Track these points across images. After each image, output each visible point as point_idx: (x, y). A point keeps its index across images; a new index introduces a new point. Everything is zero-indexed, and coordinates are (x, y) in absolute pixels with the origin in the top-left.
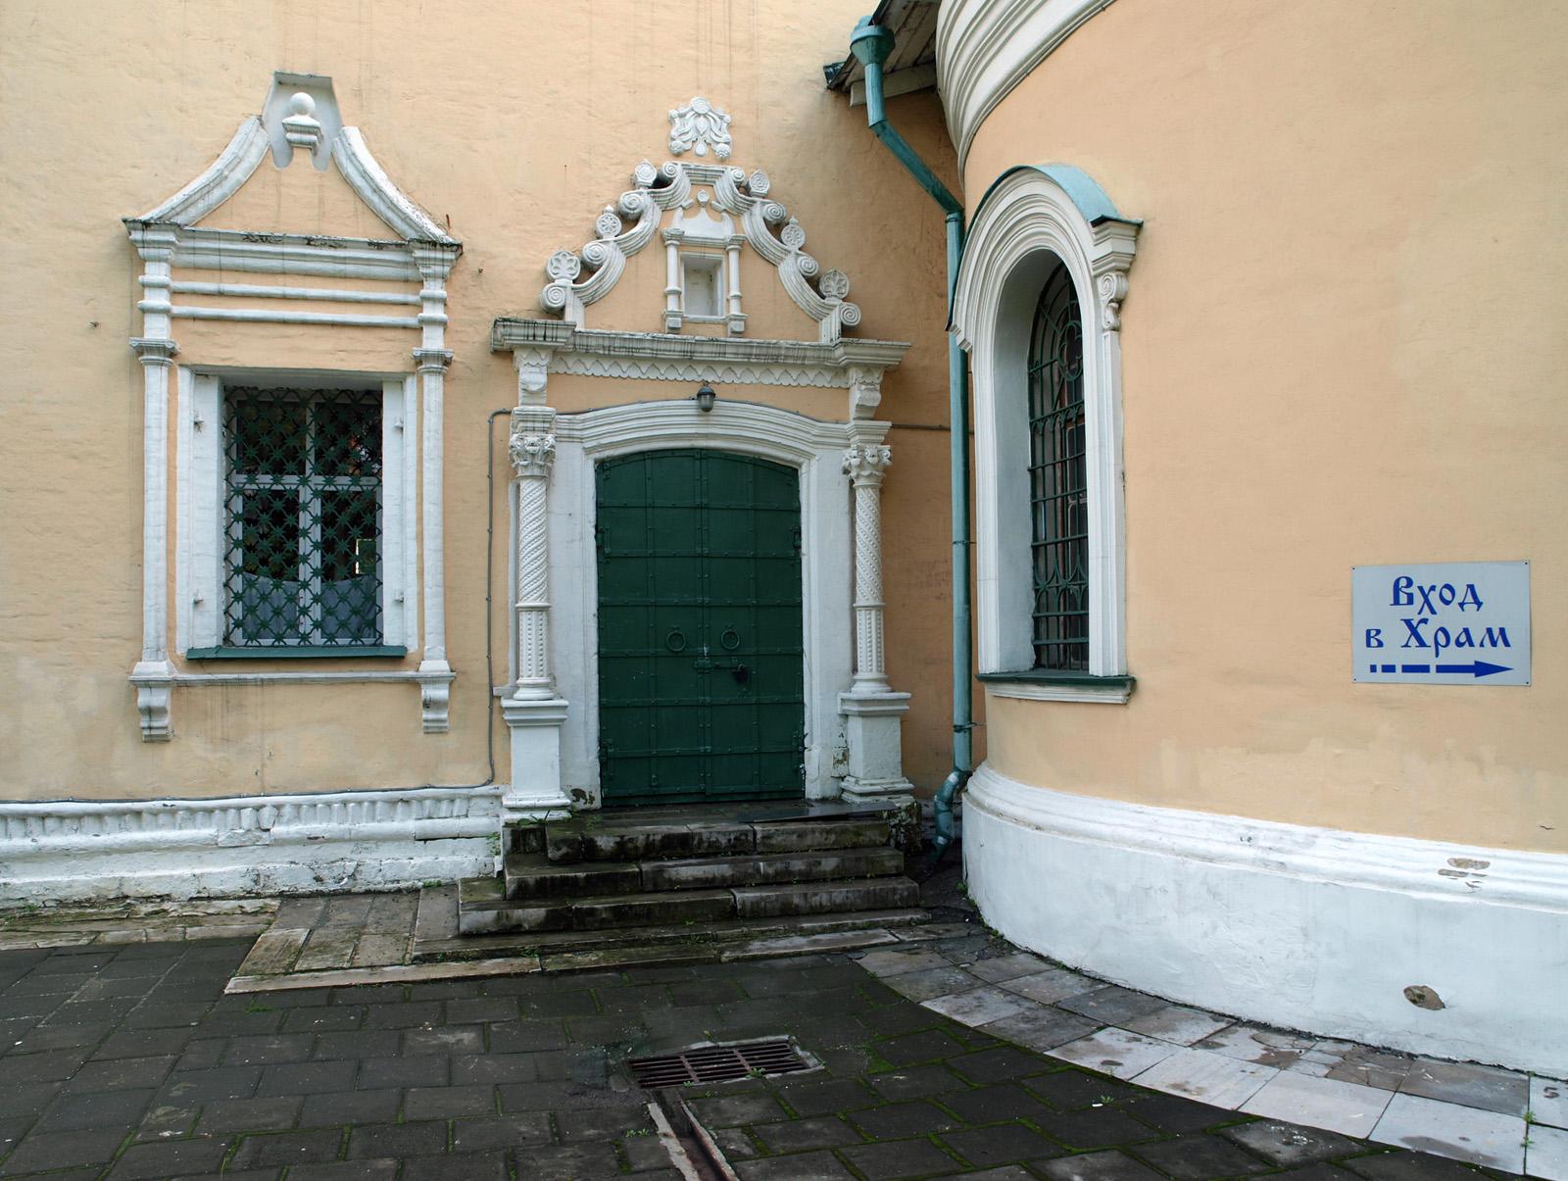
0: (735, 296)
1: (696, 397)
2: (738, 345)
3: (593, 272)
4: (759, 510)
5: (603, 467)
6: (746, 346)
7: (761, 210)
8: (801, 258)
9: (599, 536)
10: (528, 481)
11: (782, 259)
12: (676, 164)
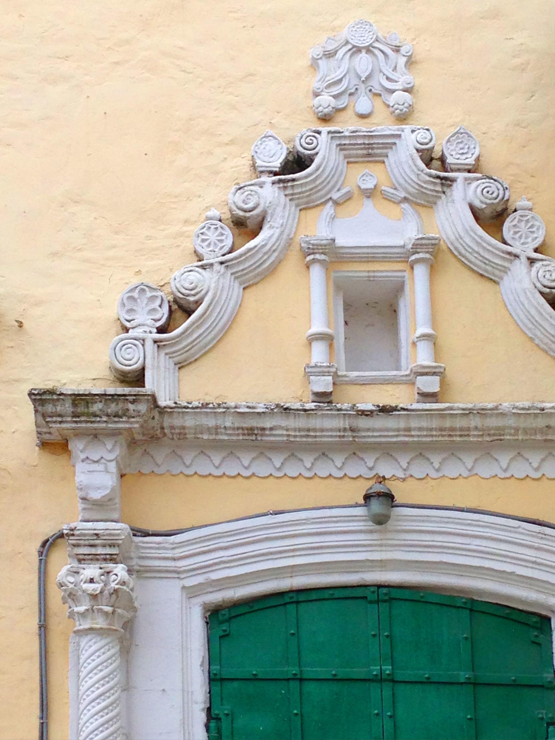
0: (425, 337)
1: (362, 502)
2: (429, 414)
3: (189, 313)
4: (478, 684)
5: (220, 618)
6: (443, 416)
7: (466, 192)
8: (538, 265)
9: (213, 724)
10: (89, 637)
11: (505, 270)
12: (319, 133)
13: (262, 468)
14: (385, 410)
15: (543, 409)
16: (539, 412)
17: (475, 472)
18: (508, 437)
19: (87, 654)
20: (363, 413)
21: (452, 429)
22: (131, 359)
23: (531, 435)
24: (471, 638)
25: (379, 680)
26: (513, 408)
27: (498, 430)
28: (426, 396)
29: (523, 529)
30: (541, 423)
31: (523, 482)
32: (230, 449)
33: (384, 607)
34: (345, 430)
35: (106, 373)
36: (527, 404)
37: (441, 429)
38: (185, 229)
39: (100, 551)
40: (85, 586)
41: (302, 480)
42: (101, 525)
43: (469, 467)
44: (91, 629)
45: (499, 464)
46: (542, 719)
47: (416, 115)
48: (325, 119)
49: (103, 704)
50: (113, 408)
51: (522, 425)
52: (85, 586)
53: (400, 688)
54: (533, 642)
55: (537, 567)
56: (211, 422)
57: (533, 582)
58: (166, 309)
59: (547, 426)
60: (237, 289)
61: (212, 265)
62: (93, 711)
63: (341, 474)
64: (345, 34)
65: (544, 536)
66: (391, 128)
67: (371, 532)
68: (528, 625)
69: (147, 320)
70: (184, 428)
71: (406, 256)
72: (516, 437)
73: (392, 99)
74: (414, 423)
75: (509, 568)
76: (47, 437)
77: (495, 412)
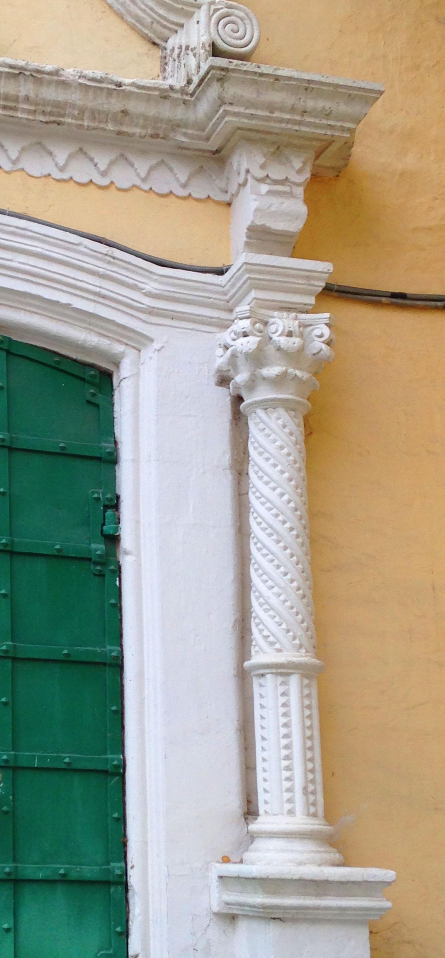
15: (120, 85)
16: (114, 87)
17: (20, 166)
18: (69, 120)
23: (100, 122)
24: (8, 389)
26: (79, 77)
27: (57, 107)
29: (86, 247)
30: (115, 105)
31: (83, 189)
36: (99, 74)
43: (14, 157)
45: (53, 159)
46: (98, 499)
51: (90, 105)
54: (89, 402)
55: (101, 300)
57: (94, 321)
59: (123, 112)
65: (112, 260)
68: (83, 380)
72: (80, 122)
75: (64, 299)
77: (55, 78)
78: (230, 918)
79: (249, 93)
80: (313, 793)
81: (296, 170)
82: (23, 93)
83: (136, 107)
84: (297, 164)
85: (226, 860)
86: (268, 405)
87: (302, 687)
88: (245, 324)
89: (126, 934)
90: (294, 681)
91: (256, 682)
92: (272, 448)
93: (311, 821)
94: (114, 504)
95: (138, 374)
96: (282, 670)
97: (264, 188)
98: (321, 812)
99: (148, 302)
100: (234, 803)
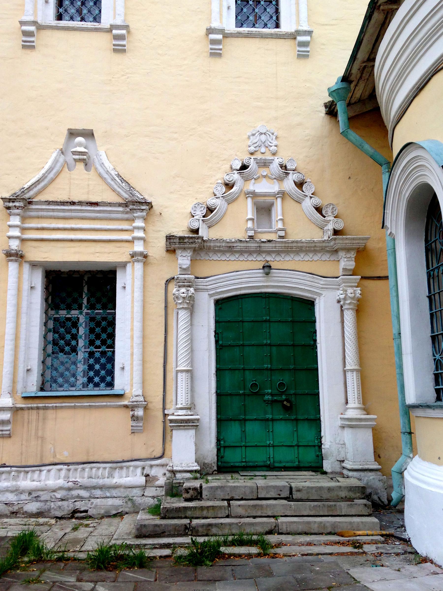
5: (218, 303)
7: (293, 177)
8: (313, 199)
11: (303, 200)
13: (232, 258)
14: (269, 241)
19: (181, 315)
20: (263, 242)
21: (288, 247)
22: (195, 225)
25: (266, 321)
28: (281, 237)
30: (313, 245)
32: (223, 252)
33: (267, 299)
34: (257, 247)
35: (185, 228)
36: (309, 239)
37: (285, 247)
38: (210, 186)
39: (186, 284)
40: (181, 295)
41: (244, 261)
42: (186, 276)
44: (183, 308)
47: (278, 153)
48: (252, 154)
49: (186, 330)
50: (191, 241)
52: (181, 295)
53: (272, 324)
56: (218, 244)
58: (205, 210)
60: (226, 204)
61: (219, 197)
62: (183, 333)
63: (255, 260)
64: (258, 129)
66: (272, 158)
67: (264, 277)
69: (199, 213)
70: (210, 246)
71: (275, 195)
73: (271, 149)
74: (278, 245)
75: (303, 287)
76: (169, 249)
78: (343, 427)
79: (341, 242)
80: (360, 398)
81: (353, 255)
82: (294, 245)
83: (317, 245)
84: (353, 253)
85: (342, 414)
86: (348, 309)
87: (356, 374)
88: (342, 292)
89: (320, 431)
90: (355, 373)
91: (347, 373)
92: (349, 319)
93: (359, 405)
94: (315, 332)
95: (320, 302)
96: (352, 371)
97: (346, 259)
98: (361, 402)
99: (321, 286)
100: (343, 401)
